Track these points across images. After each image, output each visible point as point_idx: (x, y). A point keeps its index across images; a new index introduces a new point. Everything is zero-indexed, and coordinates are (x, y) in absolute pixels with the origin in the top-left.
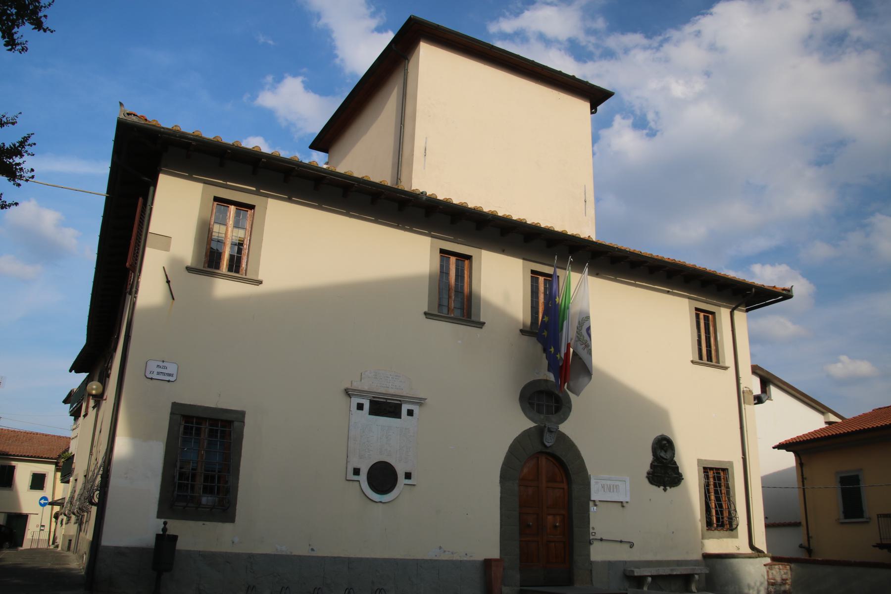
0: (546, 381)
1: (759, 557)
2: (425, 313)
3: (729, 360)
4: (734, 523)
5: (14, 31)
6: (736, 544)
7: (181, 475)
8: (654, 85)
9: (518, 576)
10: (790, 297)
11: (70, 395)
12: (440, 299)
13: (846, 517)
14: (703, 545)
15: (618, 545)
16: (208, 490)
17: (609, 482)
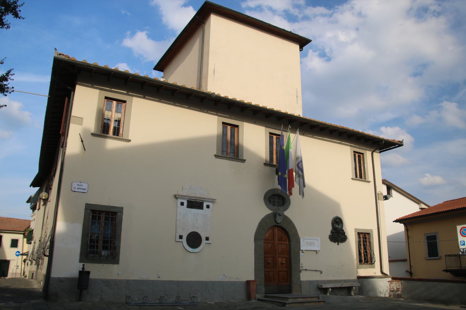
0: (277, 189)
1: (385, 277)
2: (215, 155)
3: (371, 178)
4: (373, 261)
6: (374, 271)
7: (91, 241)
8: (329, 34)
9: (264, 289)
10: (402, 145)
13: (429, 257)
14: (357, 272)
15: (315, 272)
16: (105, 248)
17: (310, 241)
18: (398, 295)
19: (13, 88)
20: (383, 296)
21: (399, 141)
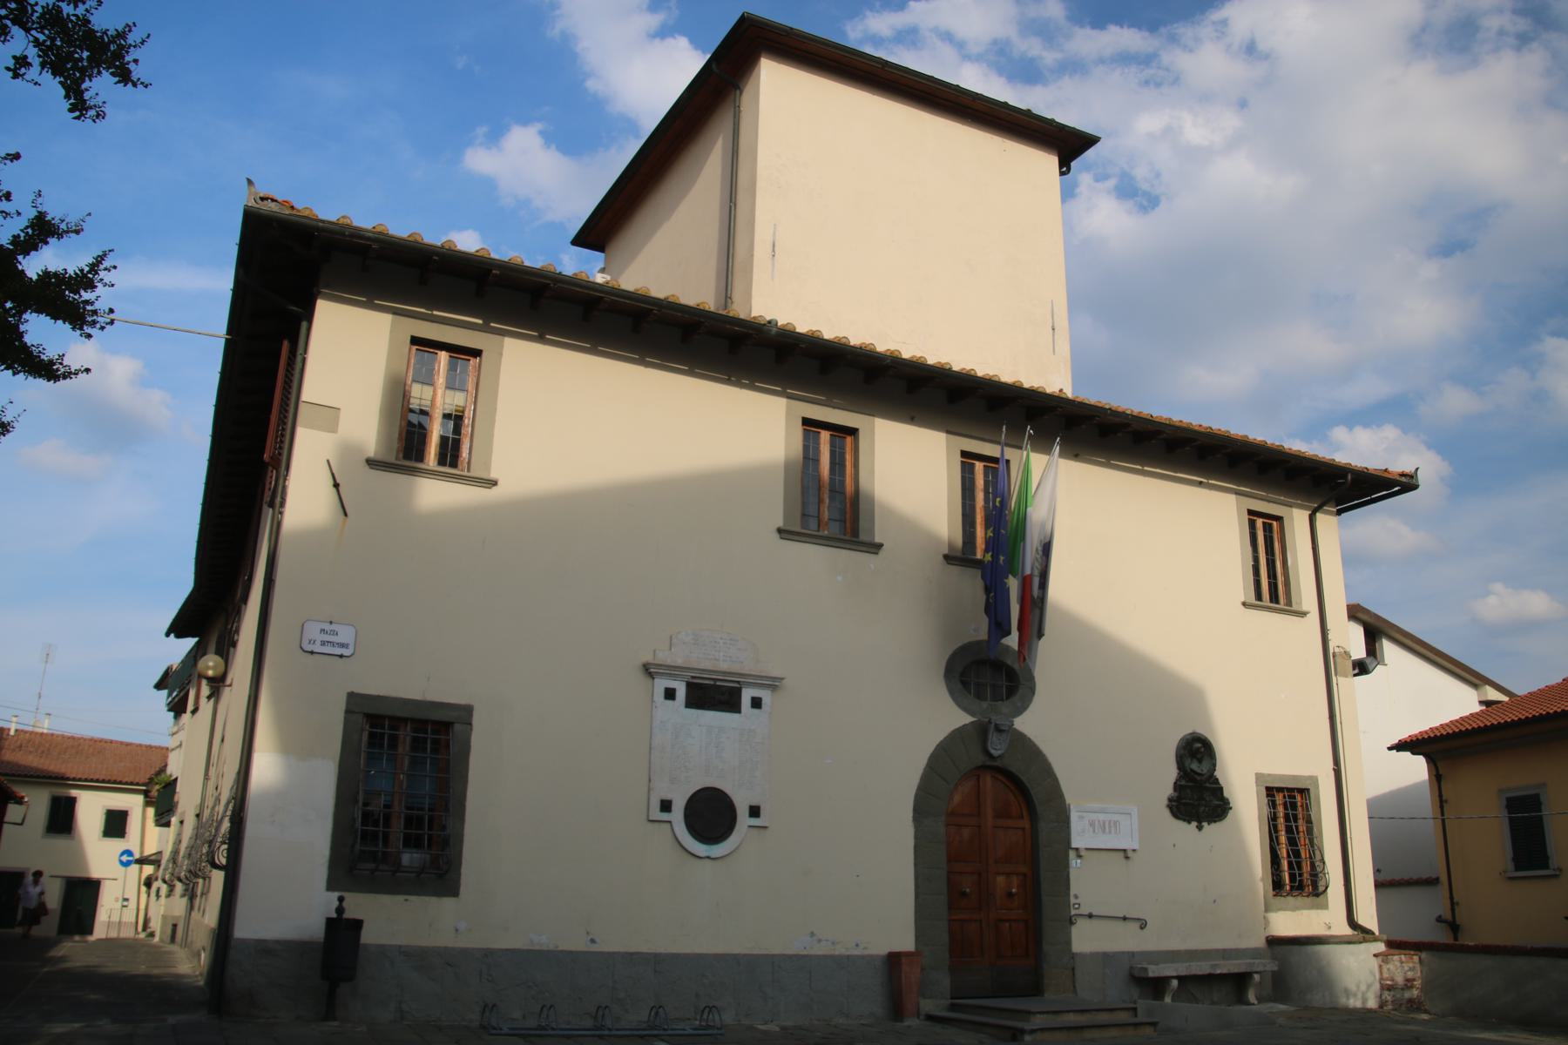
1: (1365, 941)
2: (780, 531)
3: (1308, 600)
5: (84, 86)
6: (1325, 919)
7: (366, 816)
10: (1414, 487)
11: (167, 674)
12: (804, 504)
13: (1517, 868)
14: (1267, 922)
15: (1121, 923)
16: (412, 842)
17: (1102, 817)
18: (1410, 1001)
19: (111, 311)
20: (1359, 1004)
21: (1403, 475)
